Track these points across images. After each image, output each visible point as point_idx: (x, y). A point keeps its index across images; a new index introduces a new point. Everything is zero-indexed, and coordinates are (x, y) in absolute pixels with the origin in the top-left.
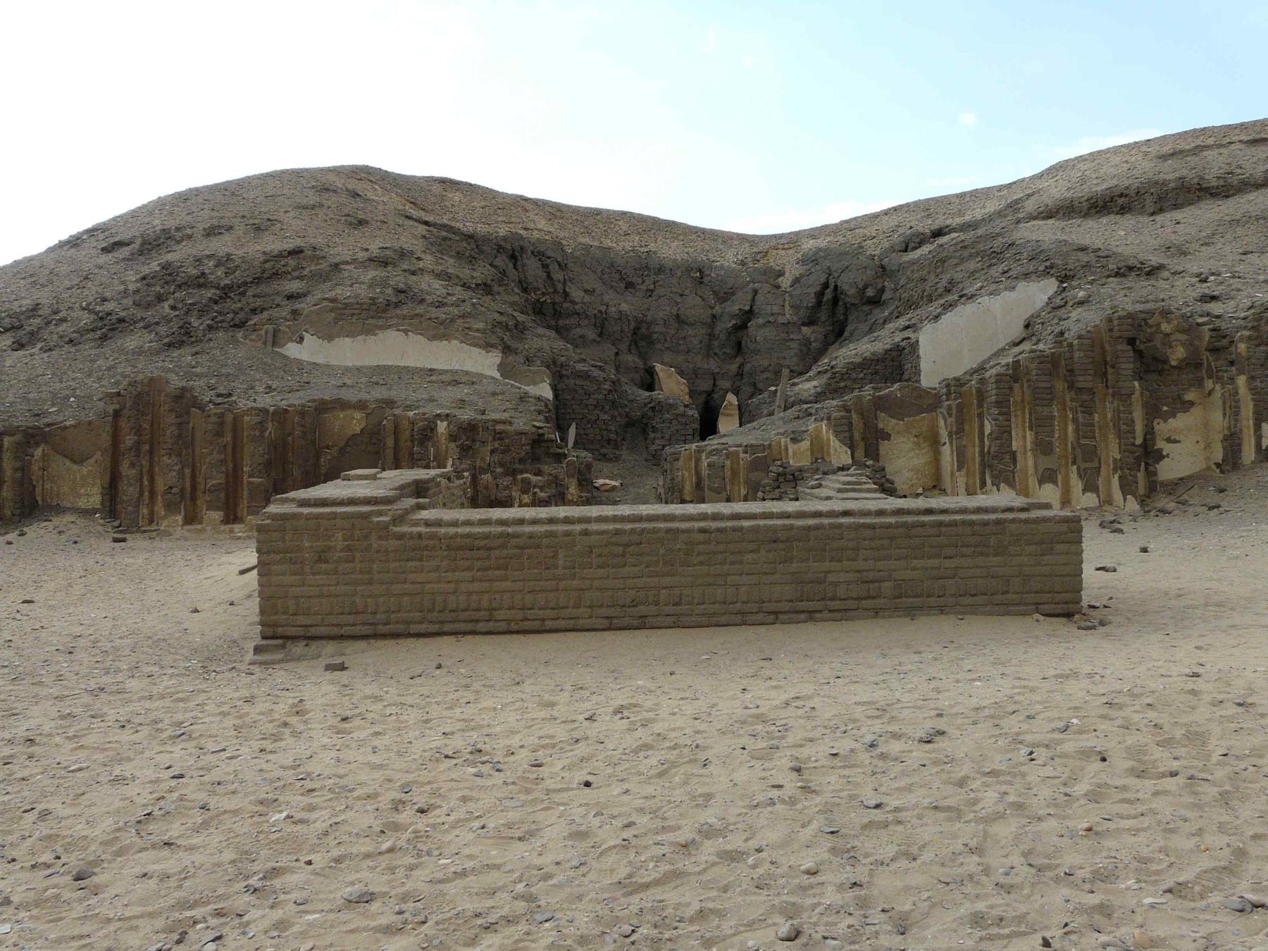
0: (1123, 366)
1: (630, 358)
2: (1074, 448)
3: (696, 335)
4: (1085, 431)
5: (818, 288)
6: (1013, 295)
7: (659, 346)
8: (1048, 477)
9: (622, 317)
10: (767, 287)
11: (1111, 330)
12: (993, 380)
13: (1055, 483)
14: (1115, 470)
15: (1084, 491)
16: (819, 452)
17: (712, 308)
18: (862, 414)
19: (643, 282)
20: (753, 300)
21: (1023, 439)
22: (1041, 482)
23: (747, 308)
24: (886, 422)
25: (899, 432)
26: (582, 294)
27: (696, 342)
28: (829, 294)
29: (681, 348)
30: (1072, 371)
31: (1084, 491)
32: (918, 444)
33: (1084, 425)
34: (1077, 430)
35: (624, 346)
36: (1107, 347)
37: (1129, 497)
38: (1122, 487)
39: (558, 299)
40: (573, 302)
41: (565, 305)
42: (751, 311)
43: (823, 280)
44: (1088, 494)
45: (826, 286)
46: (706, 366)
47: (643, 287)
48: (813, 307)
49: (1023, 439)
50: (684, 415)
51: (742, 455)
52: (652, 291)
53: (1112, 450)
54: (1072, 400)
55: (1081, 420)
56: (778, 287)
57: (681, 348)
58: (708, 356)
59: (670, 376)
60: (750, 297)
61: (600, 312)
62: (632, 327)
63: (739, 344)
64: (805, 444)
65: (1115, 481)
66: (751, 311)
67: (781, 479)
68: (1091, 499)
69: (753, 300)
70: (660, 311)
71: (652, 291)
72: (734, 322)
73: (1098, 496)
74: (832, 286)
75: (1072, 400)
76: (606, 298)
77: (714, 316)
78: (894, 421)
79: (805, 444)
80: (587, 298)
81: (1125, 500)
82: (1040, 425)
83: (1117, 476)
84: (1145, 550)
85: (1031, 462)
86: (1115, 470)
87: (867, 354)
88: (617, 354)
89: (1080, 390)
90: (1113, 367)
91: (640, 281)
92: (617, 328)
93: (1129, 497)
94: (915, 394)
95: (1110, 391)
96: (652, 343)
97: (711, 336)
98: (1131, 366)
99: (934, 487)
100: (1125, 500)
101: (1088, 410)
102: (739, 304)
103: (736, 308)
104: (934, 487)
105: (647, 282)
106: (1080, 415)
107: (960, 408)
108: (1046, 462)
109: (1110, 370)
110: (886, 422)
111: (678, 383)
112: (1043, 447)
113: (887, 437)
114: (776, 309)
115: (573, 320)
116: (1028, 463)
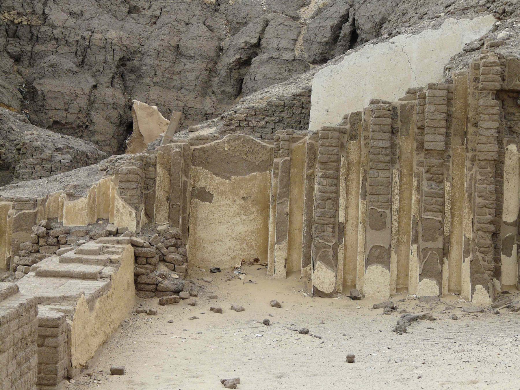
0: (484, 125)
1: (110, 91)
2: (416, 224)
3: (192, 70)
4: (435, 202)
5: (335, 22)
6: (436, 34)
7: (147, 80)
8: (379, 256)
9: (107, 46)
10: (281, 18)
11: (476, 80)
12: (9, 126)
13: (387, 264)
14: (467, 252)
15: (422, 275)
16: (100, 214)
17: (220, 39)
18: (169, 170)
19: (150, 7)
20: (263, 32)
21: (353, 209)
22: (369, 262)
23: (254, 41)
24: (206, 179)
25: (223, 193)
26: (66, 16)
27: (191, 77)
28: (346, 29)
29: (175, 83)
30: (421, 128)
31: (422, 275)
32: (245, 208)
33: (428, 195)
34: (419, 201)
35: (104, 79)
36: (470, 100)
37: (478, 287)
38: (473, 273)
39: (36, 21)
40: (52, 26)
41: (44, 29)
42: (258, 45)
43: (343, 12)
44: (426, 280)
45: (345, 18)
46: (198, 106)
47: (149, 13)
48: (327, 43)
49: (353, 209)
50: (50, 160)
51: (11, 211)
52: (157, 17)
53: (465, 228)
54: (420, 164)
55: (425, 189)
56: (295, 18)
57: (175, 83)
58: (204, 95)
59: (151, 114)
60: (259, 28)
61: (83, 38)
62: (117, 58)
63: (241, 81)
64: (83, 202)
65: (466, 267)
66: (258, 45)
67: (42, 242)
68: (428, 287)
69: (263, 32)
70: (157, 39)
71: (157, 17)
72: (237, 56)
73: (440, 284)
74: (350, 20)
75: (420, 164)
76: (94, 23)
77: (221, 49)
78: (218, 179)
79: (83, 202)
80: (71, 22)
81: (473, 290)
82: (377, 194)
83: (468, 260)
84: (351, 360)
85: (360, 237)
86: (467, 252)
87: (274, 99)
88: (95, 87)
89: (429, 152)
90: (476, 125)
91: (147, 5)
92: (100, 58)
93: (478, 287)
94: (246, 149)
95: (470, 155)
96: (140, 77)
97: (212, 71)
98: (496, 125)
99: (256, 261)
100: (473, 290)
101: (437, 178)
102: (248, 36)
103: (242, 40)
104: (256, 261)
105: (154, 7)
106: (425, 183)
107: (288, 167)
108: (381, 238)
109: (471, 129)
110: (206, 179)
111: (160, 123)
112: (376, 221)
113: (205, 196)
114: (284, 43)
115: (49, 46)
116: (357, 238)
